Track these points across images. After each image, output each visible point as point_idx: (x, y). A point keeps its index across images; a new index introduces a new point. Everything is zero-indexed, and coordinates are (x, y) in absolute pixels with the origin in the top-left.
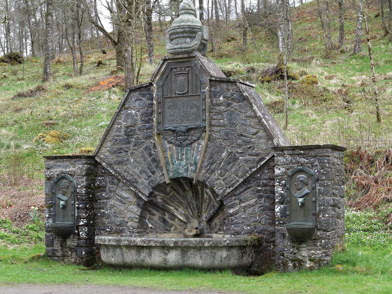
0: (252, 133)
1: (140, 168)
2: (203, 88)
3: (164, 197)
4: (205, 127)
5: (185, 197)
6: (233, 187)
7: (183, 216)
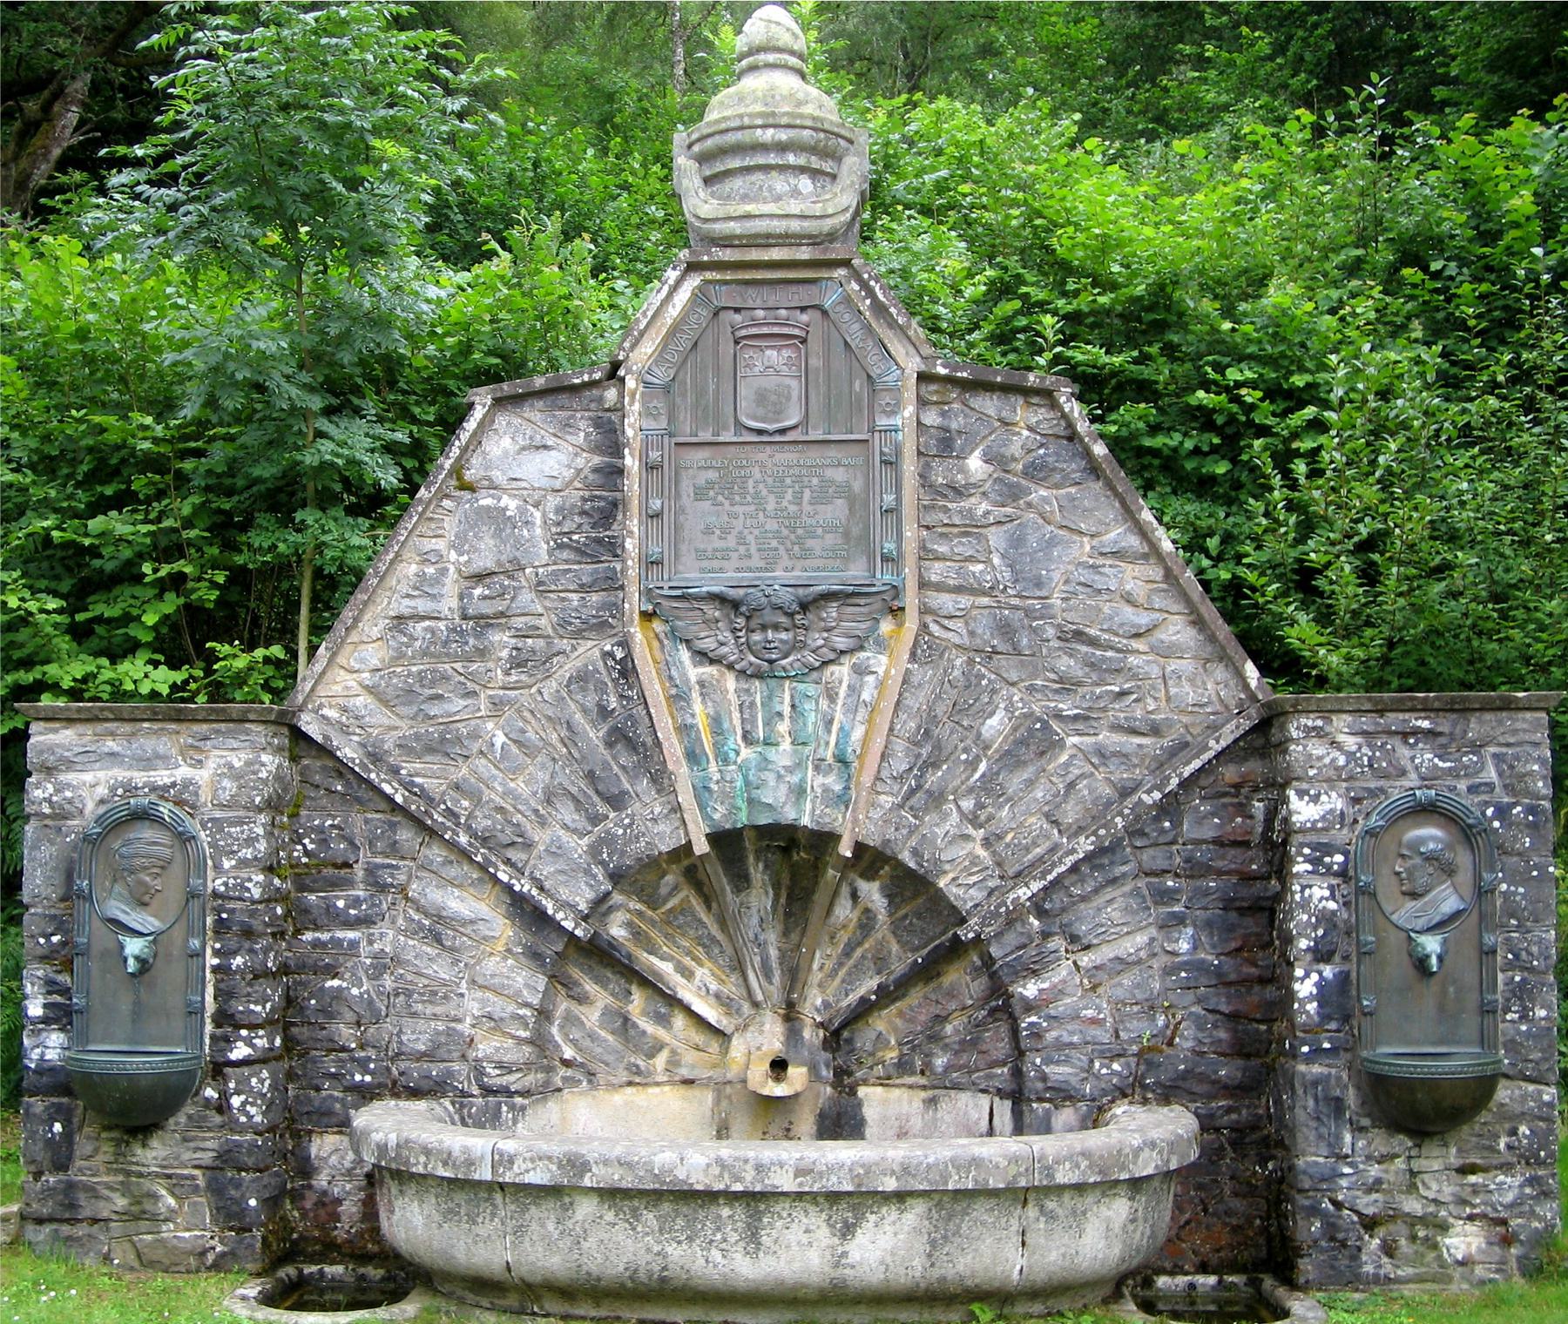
0: (1134, 631)
2: (884, 412)
3: (640, 914)
4: (896, 591)
7: (712, 1000)
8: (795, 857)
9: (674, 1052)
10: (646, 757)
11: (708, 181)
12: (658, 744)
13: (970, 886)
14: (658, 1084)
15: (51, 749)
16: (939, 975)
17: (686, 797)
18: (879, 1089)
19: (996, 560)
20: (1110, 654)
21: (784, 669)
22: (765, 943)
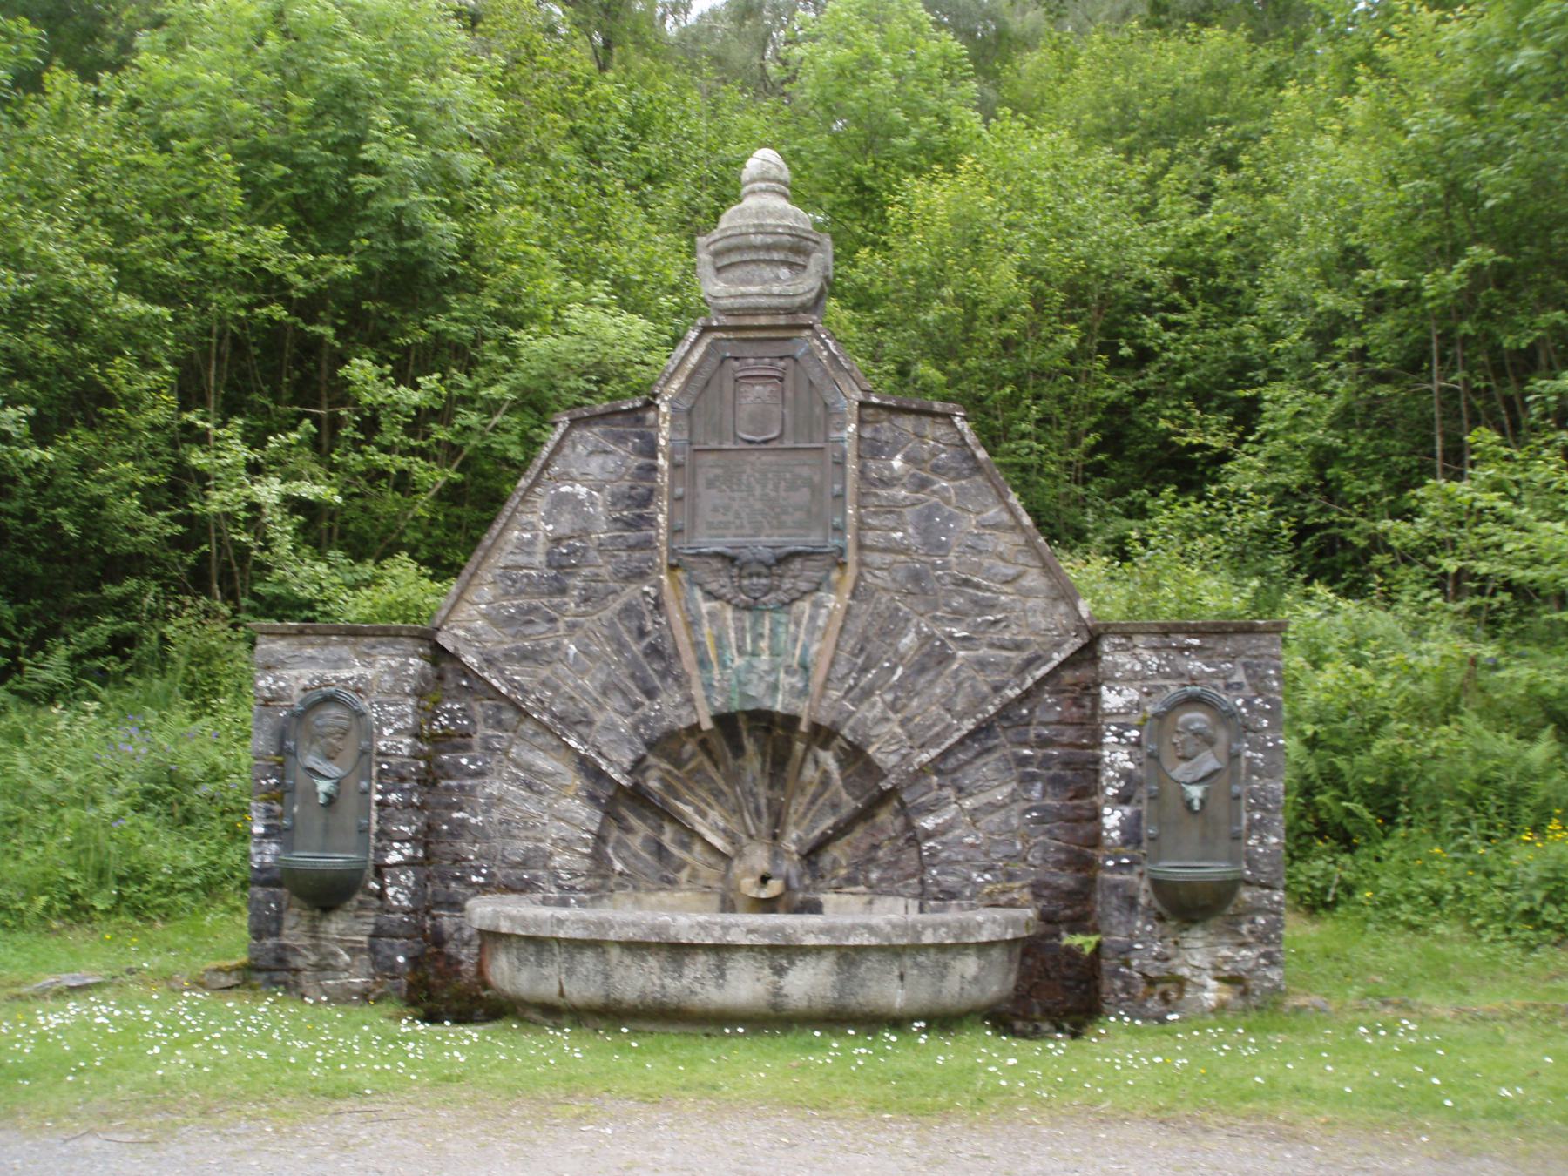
1: (601, 676)
3: (669, 772)
4: (842, 551)
5: (733, 777)
6: (938, 746)
11: (719, 270)
15: (270, 653)
17: (697, 692)
20: (988, 594)
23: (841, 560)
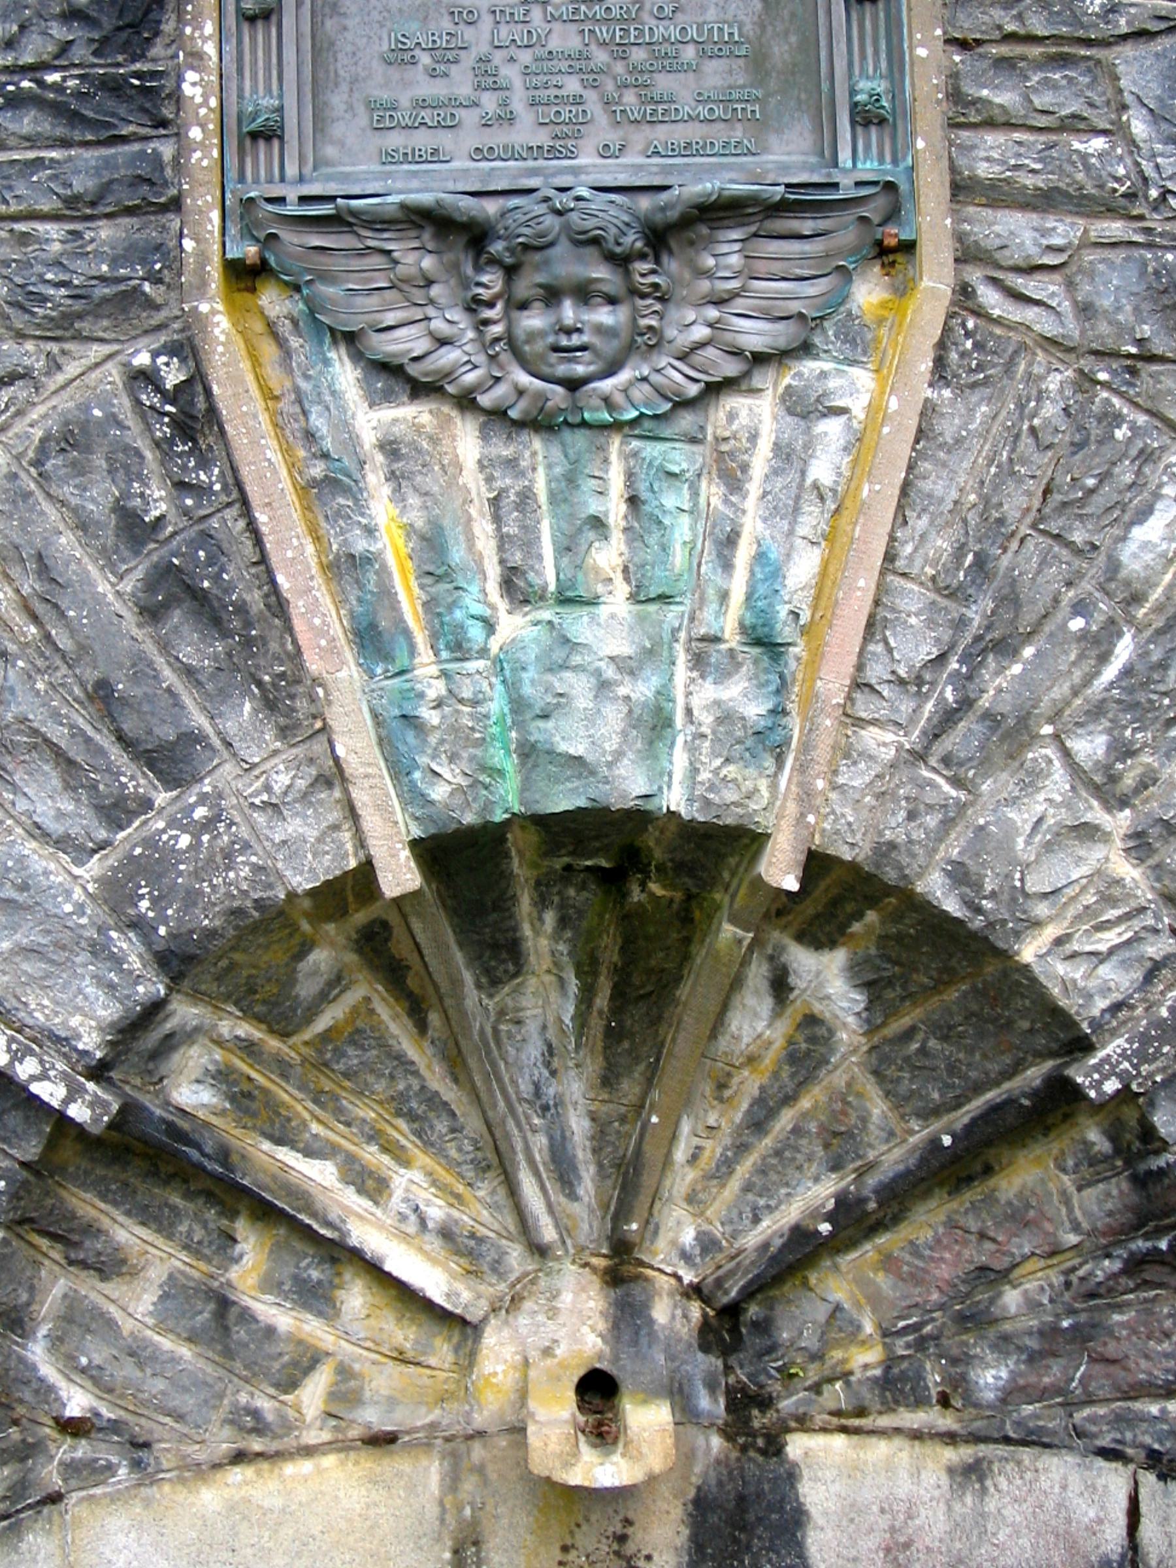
3: (249, 1048)
7: (434, 1244)
8: (636, 895)
9: (344, 1372)
10: (248, 642)
12: (278, 606)
13: (1100, 958)
14: (308, 1451)
16: (988, 1171)
18: (839, 1441)
19: (1139, 127)
21: (607, 401)
22: (559, 1102)
23: (894, 234)
